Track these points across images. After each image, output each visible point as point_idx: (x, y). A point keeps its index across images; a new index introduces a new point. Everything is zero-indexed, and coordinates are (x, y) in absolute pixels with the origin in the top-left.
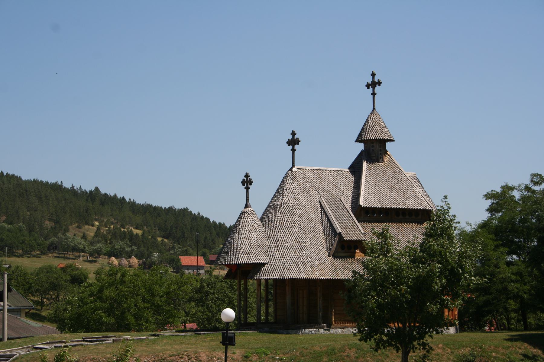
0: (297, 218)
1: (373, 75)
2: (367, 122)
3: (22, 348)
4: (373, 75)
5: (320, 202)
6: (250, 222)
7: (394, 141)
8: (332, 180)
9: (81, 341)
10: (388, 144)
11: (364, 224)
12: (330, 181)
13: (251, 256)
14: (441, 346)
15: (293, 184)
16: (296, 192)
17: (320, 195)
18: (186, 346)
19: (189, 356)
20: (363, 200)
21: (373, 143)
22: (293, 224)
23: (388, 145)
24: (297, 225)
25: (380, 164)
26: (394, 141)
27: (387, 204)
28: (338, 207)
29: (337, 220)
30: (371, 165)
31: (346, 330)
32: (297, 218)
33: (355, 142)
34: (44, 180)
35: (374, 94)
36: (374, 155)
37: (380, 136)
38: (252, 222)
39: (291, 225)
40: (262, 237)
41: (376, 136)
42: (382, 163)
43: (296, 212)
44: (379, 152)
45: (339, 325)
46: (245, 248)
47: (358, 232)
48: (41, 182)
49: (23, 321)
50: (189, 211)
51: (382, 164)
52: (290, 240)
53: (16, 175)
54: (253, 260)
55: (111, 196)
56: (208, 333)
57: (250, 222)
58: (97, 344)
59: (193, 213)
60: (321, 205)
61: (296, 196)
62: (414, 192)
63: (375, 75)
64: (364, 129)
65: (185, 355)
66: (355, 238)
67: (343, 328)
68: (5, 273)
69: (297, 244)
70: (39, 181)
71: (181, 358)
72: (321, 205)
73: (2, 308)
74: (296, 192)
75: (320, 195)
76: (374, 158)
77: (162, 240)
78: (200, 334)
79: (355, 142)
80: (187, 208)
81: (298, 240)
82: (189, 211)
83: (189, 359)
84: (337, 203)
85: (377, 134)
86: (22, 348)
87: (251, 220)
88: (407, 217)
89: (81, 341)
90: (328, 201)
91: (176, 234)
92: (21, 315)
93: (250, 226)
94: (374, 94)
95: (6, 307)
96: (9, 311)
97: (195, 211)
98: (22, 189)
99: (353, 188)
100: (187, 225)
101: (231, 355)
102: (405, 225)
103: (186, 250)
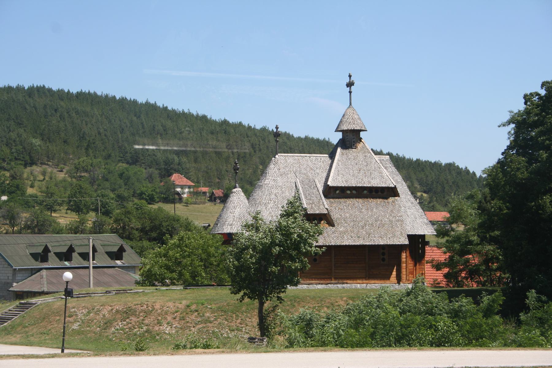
0: (273, 196)
1: (350, 76)
2: (344, 116)
3: (55, 298)
4: (350, 76)
5: (295, 183)
6: (236, 199)
7: (367, 131)
8: (310, 164)
9: (104, 293)
10: (361, 133)
11: (328, 200)
12: (308, 165)
13: (233, 227)
14: (345, 299)
15: (274, 169)
16: (276, 175)
17: (297, 177)
18: (161, 298)
19: (148, 305)
20: (331, 180)
21: (347, 133)
22: (269, 201)
23: (362, 134)
24: (273, 201)
25: (353, 150)
26: (367, 131)
27: (353, 183)
28: (310, 187)
29: (306, 197)
30: (344, 151)
31: (311, 286)
32: (273, 196)
33: (335, 131)
34: (315, 137)
35: (350, 92)
36: (348, 143)
37: (352, 127)
38: (238, 199)
39: (268, 201)
40: (244, 211)
41: (349, 127)
42: (356, 149)
43: (273, 191)
44: (353, 141)
45: (305, 282)
46: (230, 220)
47: (322, 207)
48: (313, 139)
49: (133, 277)
50: (456, 165)
51: (355, 150)
52: (265, 214)
53: (288, 132)
54: (234, 230)
55: (377, 151)
56: (193, 288)
57: (236, 199)
58: (102, 295)
59: (460, 167)
60: (296, 185)
61: (275, 178)
62: (381, 173)
63: (351, 76)
64: (341, 121)
65: (146, 305)
66: (317, 212)
67: (309, 285)
68: (90, 238)
69: (270, 217)
70: (310, 138)
71: (142, 306)
72: (296, 185)
73: (88, 266)
74: (276, 175)
75: (297, 177)
76: (348, 145)
77: (422, 195)
78: (191, 288)
79: (335, 131)
80: (454, 163)
81: (271, 214)
82: (456, 165)
83: (147, 308)
84: (312, 184)
85: (350, 125)
86: (55, 298)
87: (237, 198)
88: (374, 193)
89: (104, 293)
90: (302, 182)
91: (437, 189)
92: (135, 271)
93: (235, 203)
94: (350, 92)
95: (91, 266)
96: (94, 267)
97: (462, 166)
98: (287, 147)
99: (327, 171)
100: (449, 180)
101: (178, 304)
102: (371, 200)
103: (433, 206)
